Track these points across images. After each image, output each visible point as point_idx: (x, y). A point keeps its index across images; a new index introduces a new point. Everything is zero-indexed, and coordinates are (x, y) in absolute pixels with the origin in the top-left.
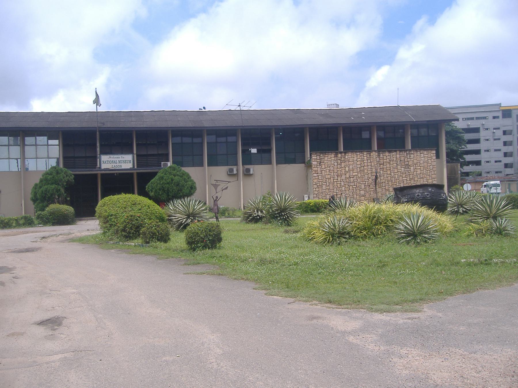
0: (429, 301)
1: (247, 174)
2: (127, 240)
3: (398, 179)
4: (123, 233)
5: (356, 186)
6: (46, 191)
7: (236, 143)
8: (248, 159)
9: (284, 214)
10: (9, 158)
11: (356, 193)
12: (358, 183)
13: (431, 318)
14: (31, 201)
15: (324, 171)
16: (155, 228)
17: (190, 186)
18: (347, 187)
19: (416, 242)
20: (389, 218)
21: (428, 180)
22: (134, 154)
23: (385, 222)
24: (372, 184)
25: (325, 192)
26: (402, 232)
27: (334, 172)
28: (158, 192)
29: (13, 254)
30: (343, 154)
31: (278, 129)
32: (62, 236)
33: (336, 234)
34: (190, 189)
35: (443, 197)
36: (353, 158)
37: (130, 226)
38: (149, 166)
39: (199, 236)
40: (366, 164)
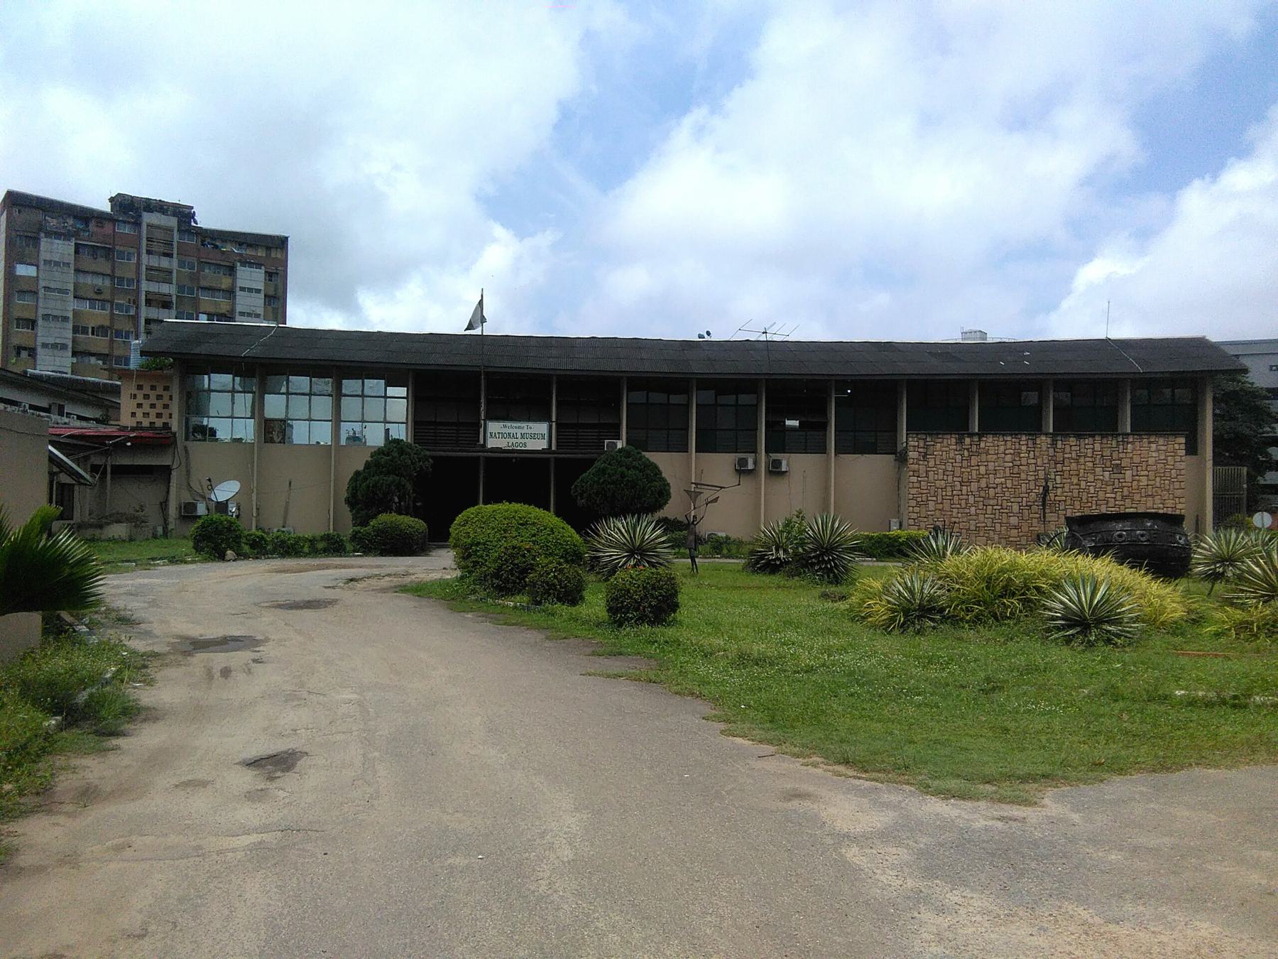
1: (775, 471)
2: (503, 596)
3: (1095, 495)
6: (375, 486)
7: (756, 407)
8: (779, 442)
9: (829, 559)
10: (310, 420)
11: (1000, 521)
13: (1053, 822)
17: (658, 491)
20: (1032, 583)
21: (1164, 500)
23: (1023, 591)
24: (1036, 503)
26: (1057, 617)
29: (278, 611)
30: (976, 439)
33: (913, 611)
35: (1179, 543)
36: (996, 448)
40: (1024, 461)
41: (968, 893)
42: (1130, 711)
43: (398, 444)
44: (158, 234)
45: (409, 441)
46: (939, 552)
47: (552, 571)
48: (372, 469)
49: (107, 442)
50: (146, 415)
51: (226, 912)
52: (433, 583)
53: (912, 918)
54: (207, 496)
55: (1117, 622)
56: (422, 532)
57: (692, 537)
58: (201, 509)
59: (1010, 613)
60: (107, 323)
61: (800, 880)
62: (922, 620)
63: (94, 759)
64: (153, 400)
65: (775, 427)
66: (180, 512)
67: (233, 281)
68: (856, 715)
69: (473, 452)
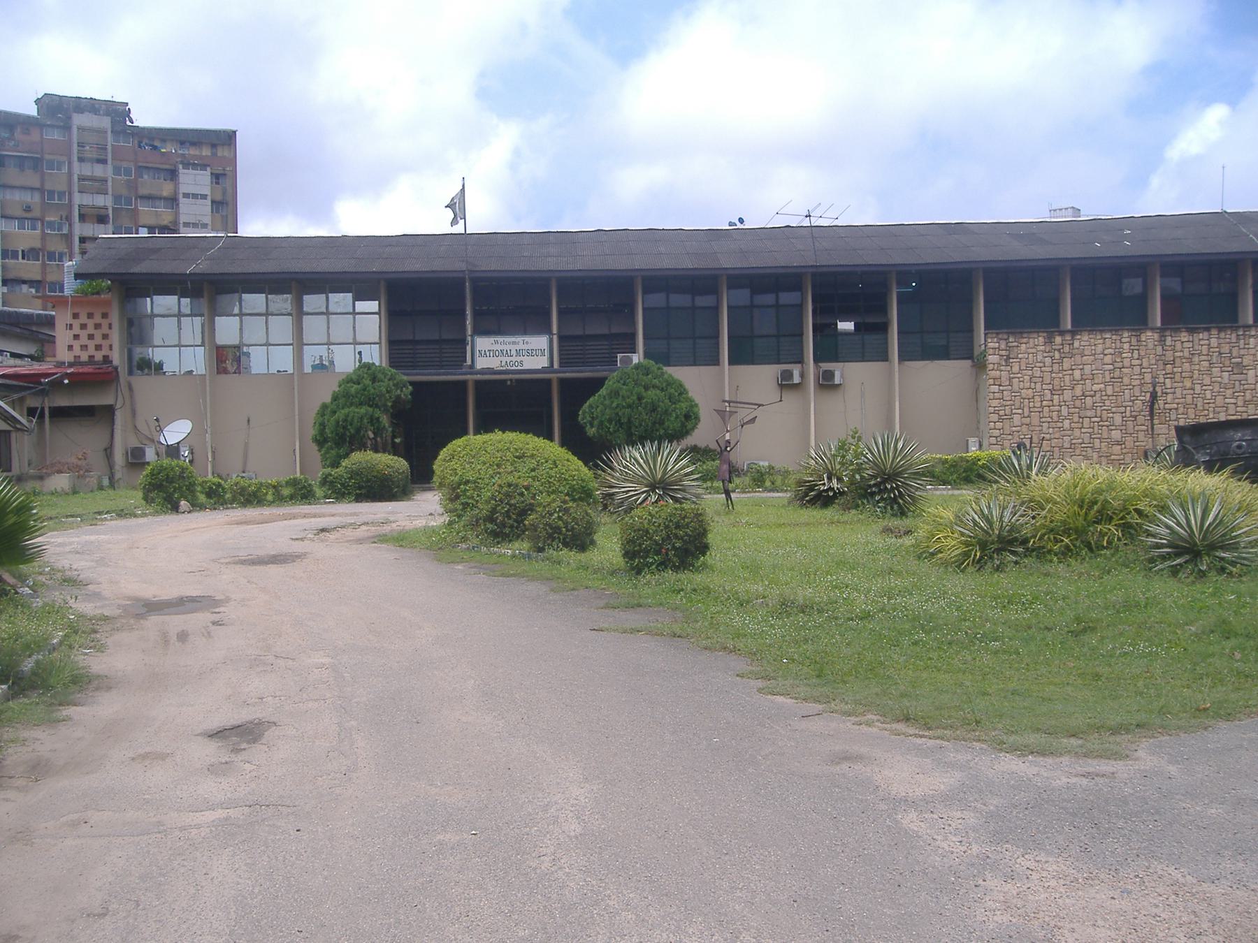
0: (1160, 730)
1: (827, 383)
2: (498, 543)
4: (490, 526)
5: (1100, 417)
6: (345, 420)
7: (800, 307)
8: (830, 348)
10: (268, 344)
11: (1099, 436)
12: (1104, 410)
14: (314, 444)
15: (1017, 379)
16: (559, 516)
18: (1076, 419)
19: (1196, 569)
20: (1133, 505)
22: (553, 334)
23: (1121, 515)
24: (1142, 413)
25: (1019, 432)
26: (1162, 544)
27: (1042, 381)
28: (606, 427)
29: (238, 567)
30: (1068, 337)
31: (904, 274)
32: (368, 528)
34: (683, 419)
36: (1093, 347)
37: (506, 509)
38: (588, 364)
39: (651, 539)
41: (1042, 857)
42: (1244, 649)
43: (369, 369)
45: (384, 365)
46: (1022, 472)
47: (555, 512)
48: (340, 401)
49: (42, 380)
50: (84, 347)
51: (193, 891)
52: (416, 530)
53: (976, 886)
54: (156, 439)
55: (1234, 547)
56: (404, 472)
57: (725, 467)
58: (150, 455)
59: (1107, 542)
60: (38, 245)
61: (847, 850)
62: (1002, 554)
63: (44, 731)
64: (91, 330)
65: (824, 330)
67: (175, 187)
68: (920, 665)
69: (459, 374)
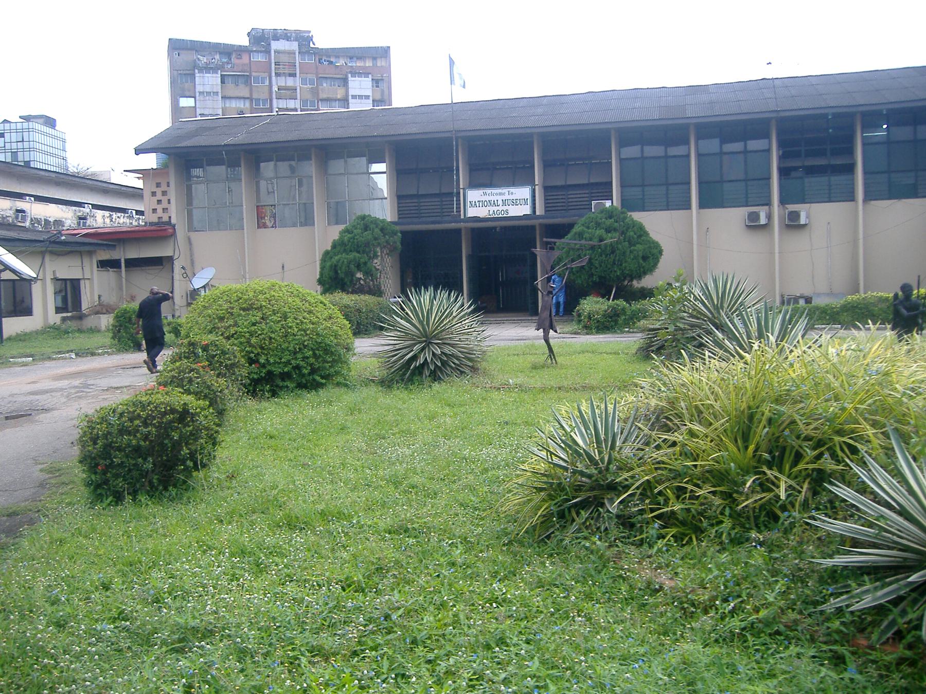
1: (793, 224)
7: (769, 151)
44: (284, 59)
66: (187, 300)
